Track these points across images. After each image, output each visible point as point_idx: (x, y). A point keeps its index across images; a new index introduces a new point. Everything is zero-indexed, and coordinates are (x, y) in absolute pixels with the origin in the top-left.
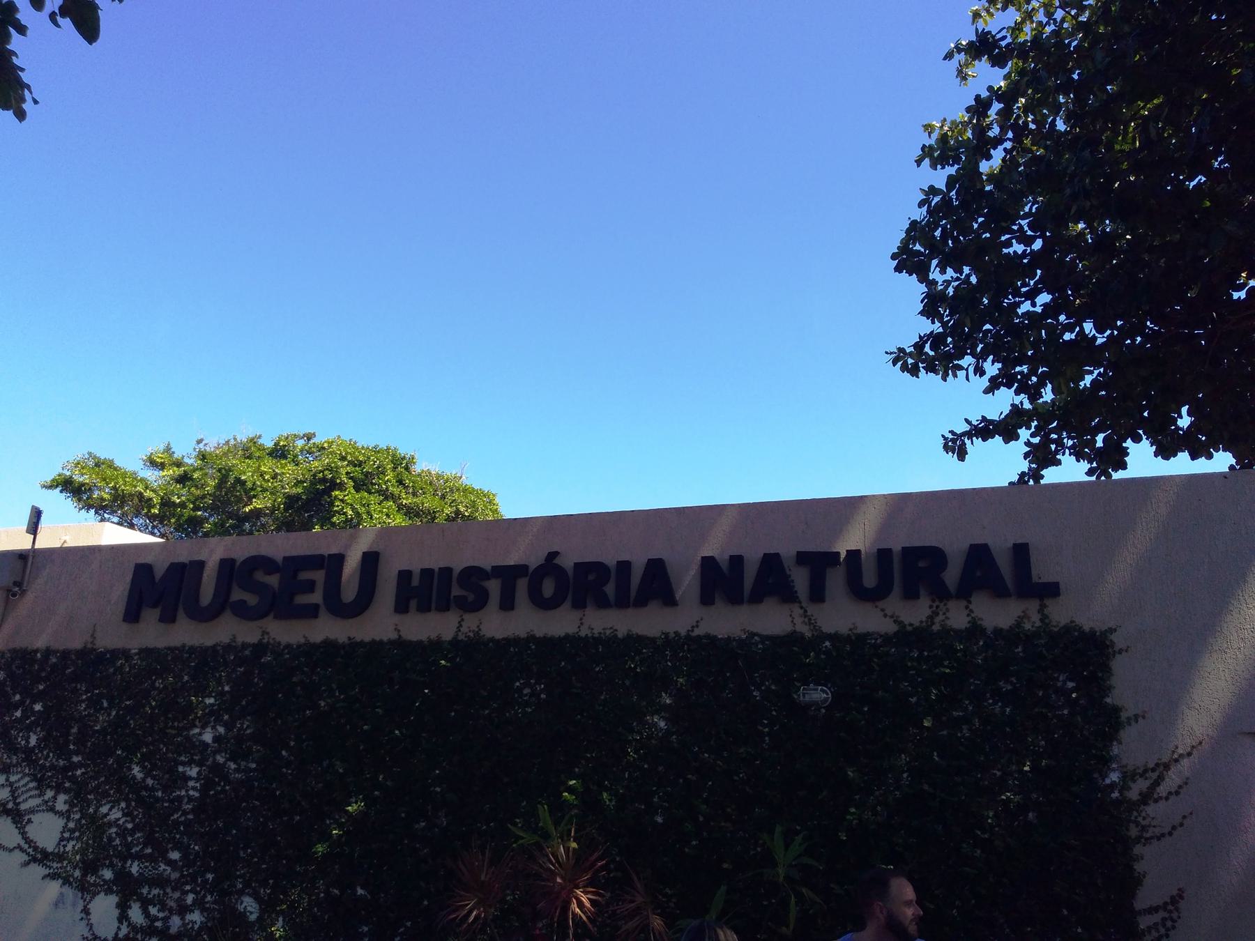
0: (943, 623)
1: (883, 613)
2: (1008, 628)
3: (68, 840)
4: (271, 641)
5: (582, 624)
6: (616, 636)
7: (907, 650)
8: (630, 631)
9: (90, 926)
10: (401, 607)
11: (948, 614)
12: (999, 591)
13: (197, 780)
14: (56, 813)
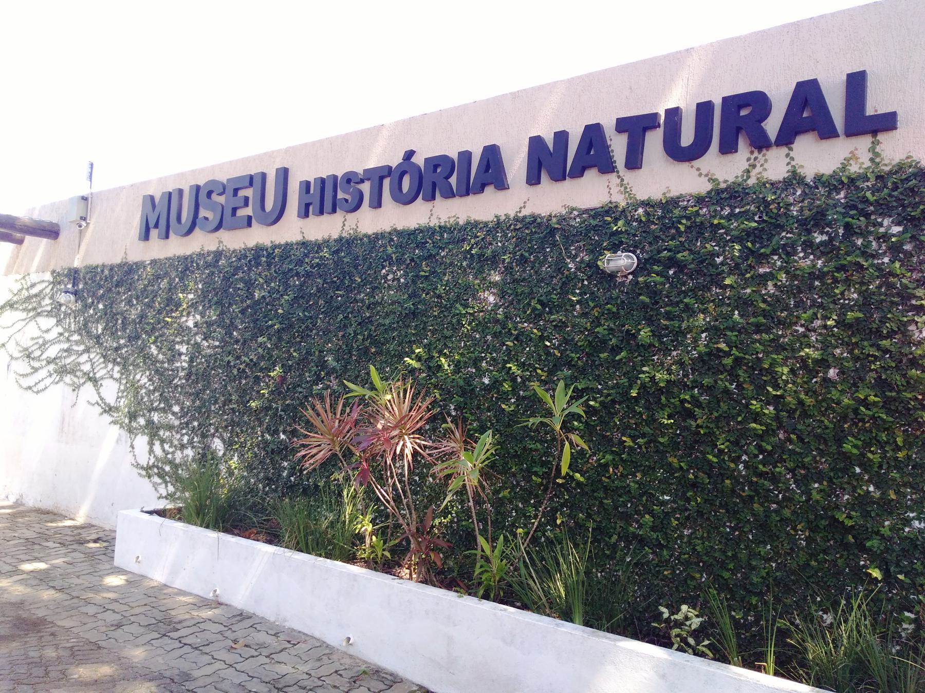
0: (759, 176)
1: (698, 173)
2: (831, 172)
3: (121, 397)
4: (225, 248)
5: (432, 215)
6: (457, 224)
7: (719, 209)
8: (469, 217)
9: (135, 456)
10: (305, 213)
11: (766, 166)
12: (827, 132)
13: (186, 355)
14: (114, 379)
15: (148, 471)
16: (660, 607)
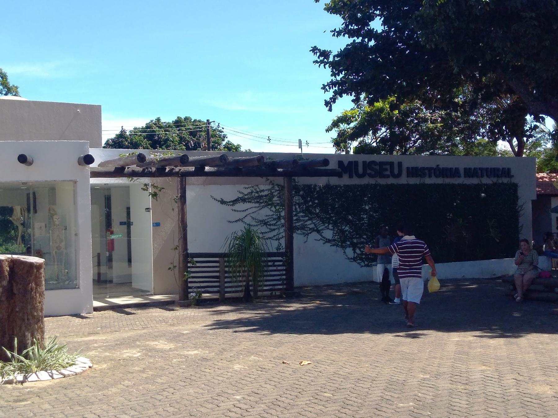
3: (335, 236)
15: (354, 259)
16: (304, 214)
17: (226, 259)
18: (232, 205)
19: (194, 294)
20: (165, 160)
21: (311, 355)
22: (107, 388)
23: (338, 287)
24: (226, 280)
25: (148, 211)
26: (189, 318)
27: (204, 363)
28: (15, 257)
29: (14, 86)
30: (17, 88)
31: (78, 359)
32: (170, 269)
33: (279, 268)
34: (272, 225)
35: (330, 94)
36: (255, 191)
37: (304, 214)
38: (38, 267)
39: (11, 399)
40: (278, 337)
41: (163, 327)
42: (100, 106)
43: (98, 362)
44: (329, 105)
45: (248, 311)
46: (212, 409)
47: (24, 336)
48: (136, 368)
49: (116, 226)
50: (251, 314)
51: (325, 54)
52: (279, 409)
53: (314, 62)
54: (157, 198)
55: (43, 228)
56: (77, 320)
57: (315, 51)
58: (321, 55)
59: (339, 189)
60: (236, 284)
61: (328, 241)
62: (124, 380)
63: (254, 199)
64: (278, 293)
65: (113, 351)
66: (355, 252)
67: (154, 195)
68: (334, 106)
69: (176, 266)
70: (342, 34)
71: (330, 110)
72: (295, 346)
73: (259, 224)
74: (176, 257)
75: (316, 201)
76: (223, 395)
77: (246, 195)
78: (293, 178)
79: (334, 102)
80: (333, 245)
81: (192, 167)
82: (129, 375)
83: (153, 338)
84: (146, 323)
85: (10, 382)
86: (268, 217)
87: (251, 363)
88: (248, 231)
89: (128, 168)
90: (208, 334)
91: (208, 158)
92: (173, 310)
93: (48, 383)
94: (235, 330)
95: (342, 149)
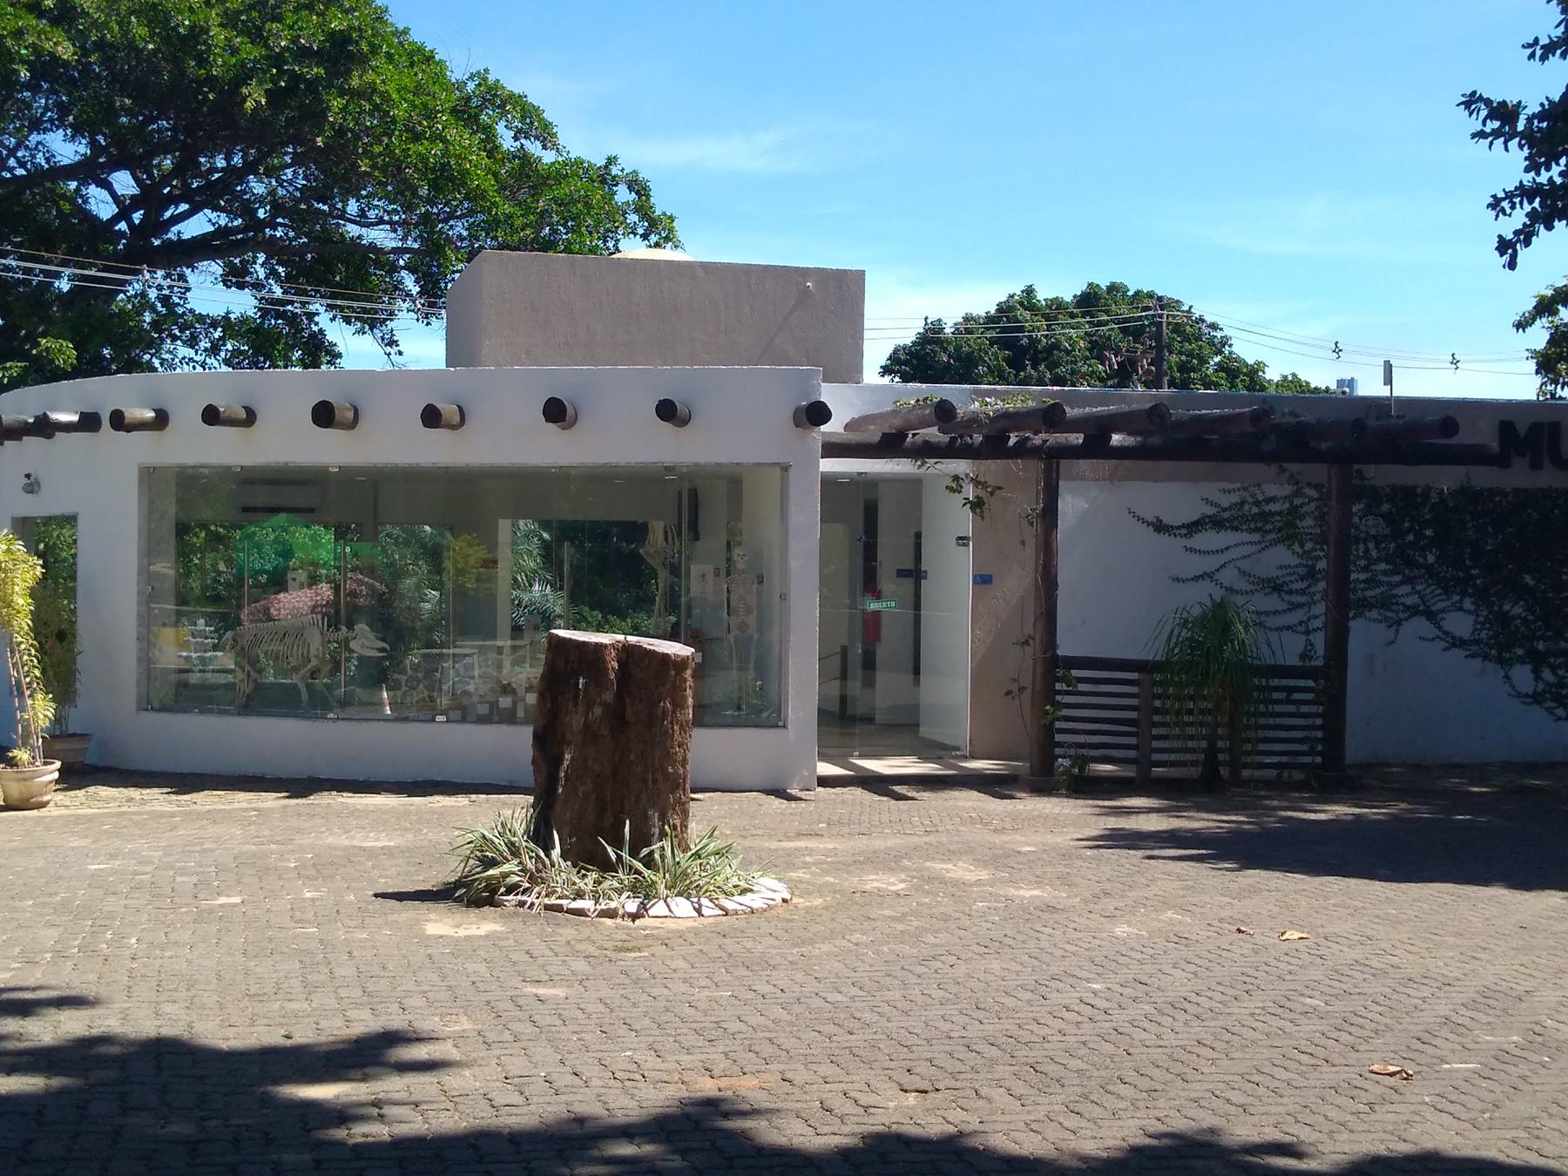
15: (1536, 698)
16: (1391, 567)
17: (1158, 677)
18: (1185, 535)
19: (1066, 762)
20: (1006, 415)
21: (1319, 922)
22: (812, 942)
23: (1479, 772)
24: (1155, 731)
25: (964, 545)
26: (1045, 819)
27: (1046, 916)
28: (632, 639)
29: (664, 214)
30: (671, 218)
31: (761, 880)
32: (1008, 693)
33: (1304, 709)
34: (1297, 592)
35: (1519, 218)
36: (1250, 500)
37: (1391, 567)
38: (681, 664)
39: (610, 945)
40: (1255, 876)
41: (979, 835)
42: (861, 274)
43: (807, 893)
44: (1510, 251)
45: (1206, 816)
46: (1029, 1002)
47: (646, 818)
48: (887, 912)
49: (886, 582)
50: (1208, 820)
51: (1504, 113)
52: (1180, 1016)
53: (1474, 136)
54: (982, 512)
55: (710, 577)
56: (776, 803)
57: (1473, 107)
58: (1491, 116)
59: (1497, 499)
60: (1176, 744)
61: (1457, 643)
62: (852, 932)
63: (1248, 520)
64: (1298, 775)
65: (845, 875)
66: (1538, 678)
67: (977, 505)
68: (1523, 254)
69: (1025, 688)
70: (1559, 52)
71: (1512, 265)
72: (1286, 899)
73: (1258, 587)
74: (1024, 664)
75: (1429, 533)
76: (1064, 979)
77: (1225, 510)
78: (1356, 466)
79: (1527, 243)
80: (1474, 656)
81: (1077, 435)
82: (866, 923)
83: (944, 855)
84: (936, 820)
85: (611, 914)
86: (1284, 572)
87: (1159, 925)
88: (1220, 607)
89: (914, 435)
90: (1080, 857)
91: (1120, 410)
92: (1012, 797)
93: (690, 923)
94: (1149, 853)
95: (1561, 380)
